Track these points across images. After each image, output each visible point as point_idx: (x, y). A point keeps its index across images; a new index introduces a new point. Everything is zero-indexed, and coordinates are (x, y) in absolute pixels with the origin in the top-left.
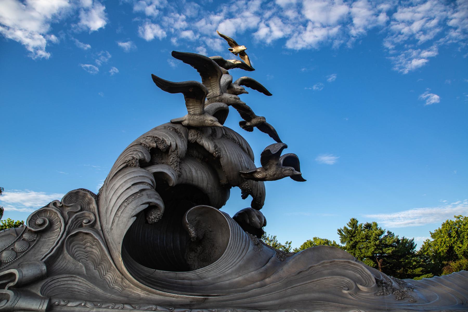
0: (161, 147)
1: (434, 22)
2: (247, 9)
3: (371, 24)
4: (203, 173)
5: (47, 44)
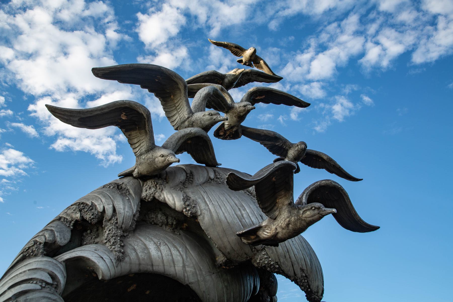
0: (88, 216)
2: (342, 32)
4: (172, 249)
5: (117, 147)
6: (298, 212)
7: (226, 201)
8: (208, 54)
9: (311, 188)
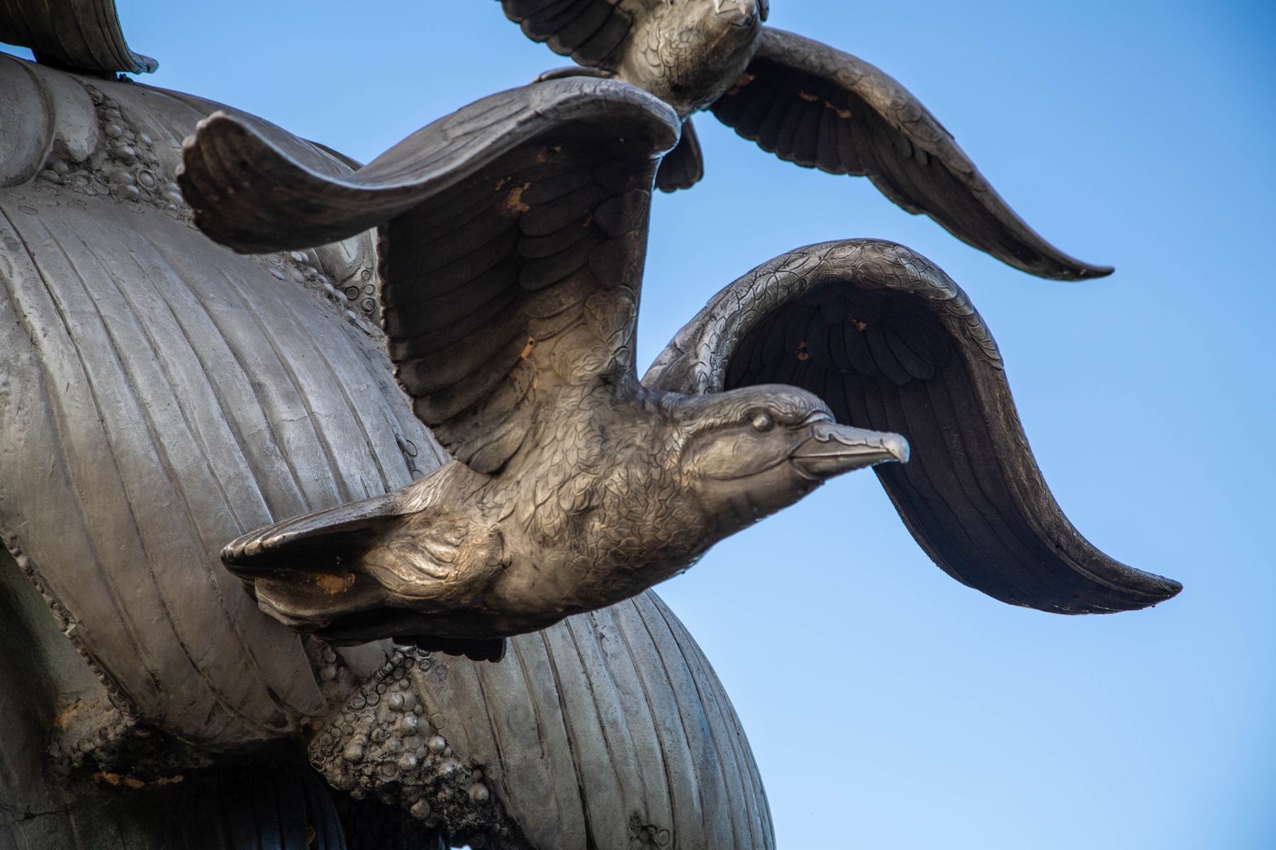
6: (657, 439)
7: (172, 326)
9: (761, 285)
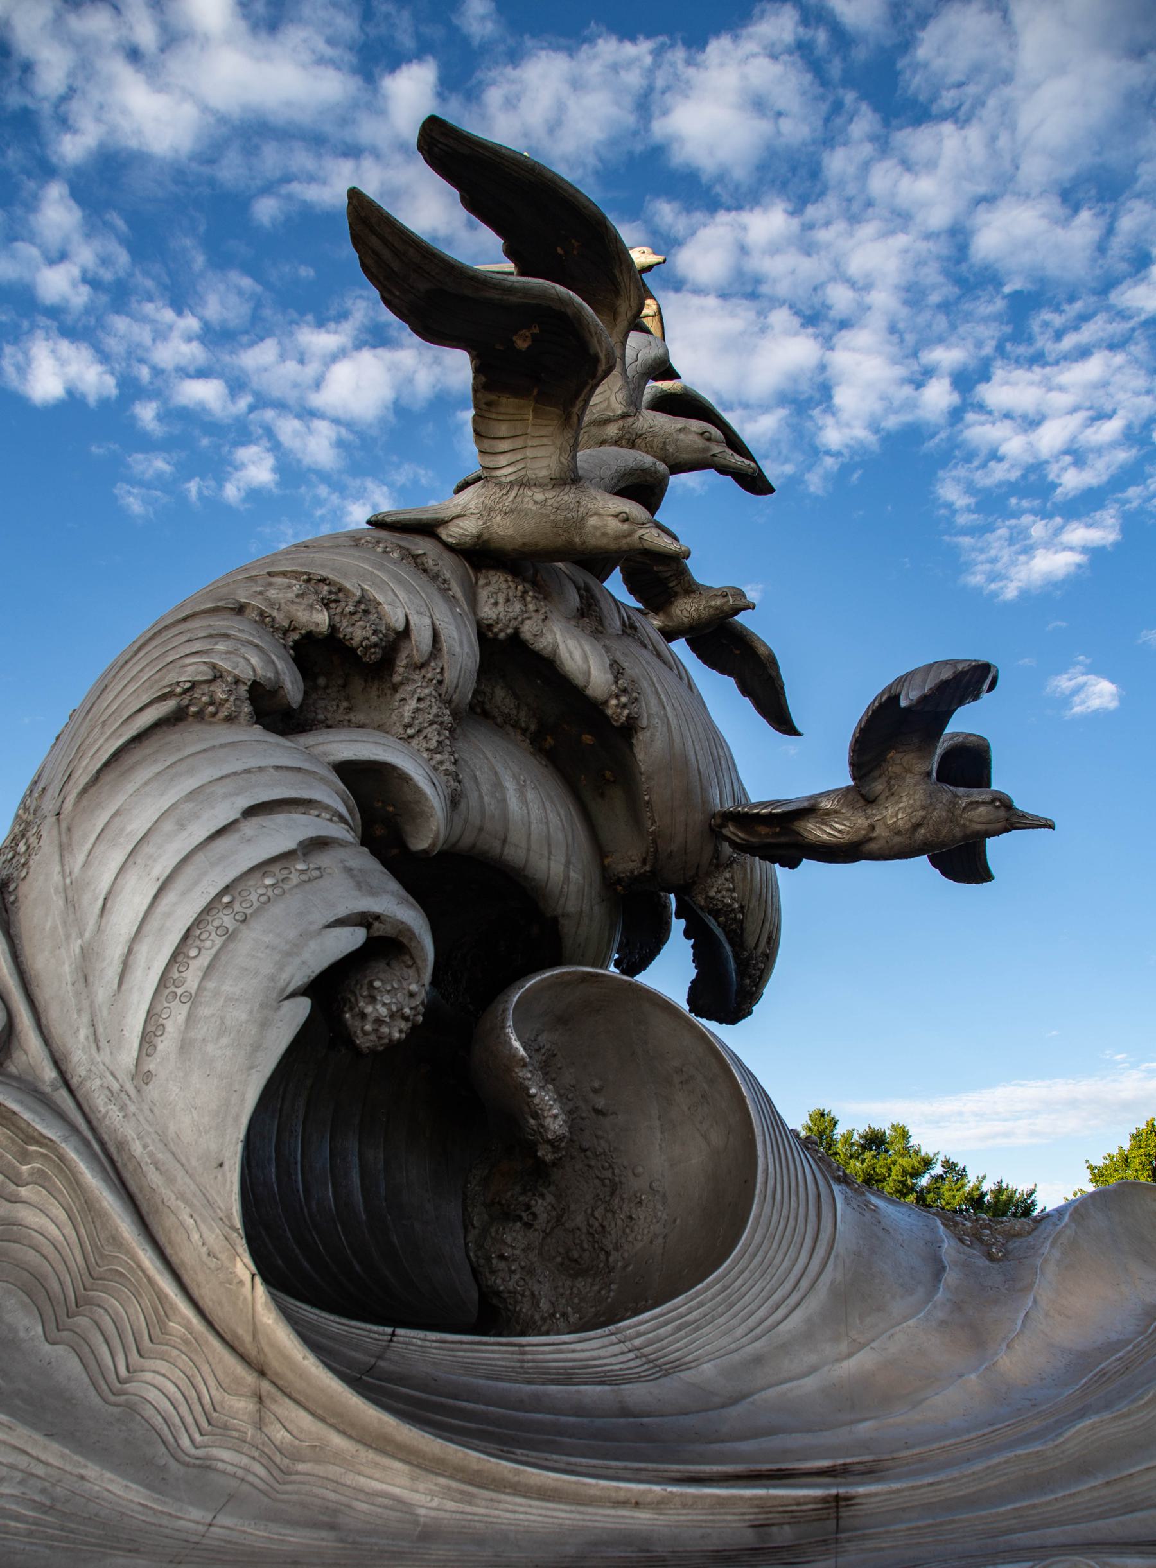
0: (358, 633)
1: (1111, 429)
3: (896, 412)
4: (548, 804)
8: (33, 205)
